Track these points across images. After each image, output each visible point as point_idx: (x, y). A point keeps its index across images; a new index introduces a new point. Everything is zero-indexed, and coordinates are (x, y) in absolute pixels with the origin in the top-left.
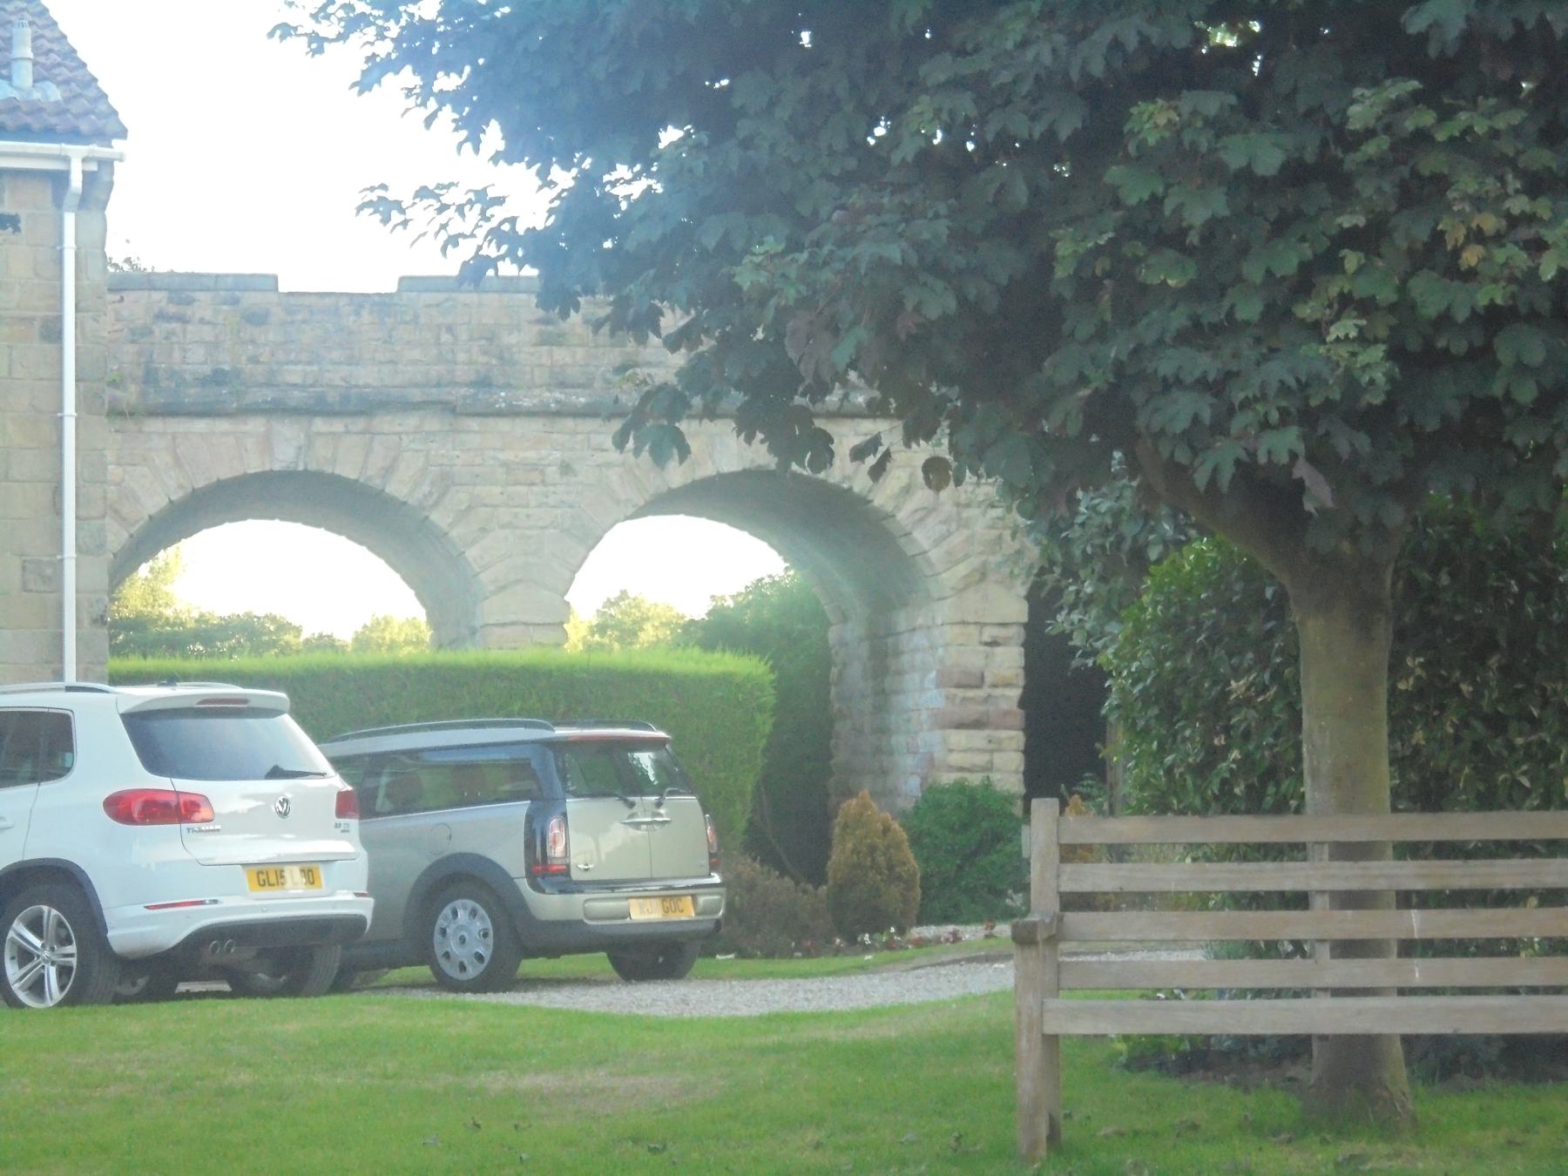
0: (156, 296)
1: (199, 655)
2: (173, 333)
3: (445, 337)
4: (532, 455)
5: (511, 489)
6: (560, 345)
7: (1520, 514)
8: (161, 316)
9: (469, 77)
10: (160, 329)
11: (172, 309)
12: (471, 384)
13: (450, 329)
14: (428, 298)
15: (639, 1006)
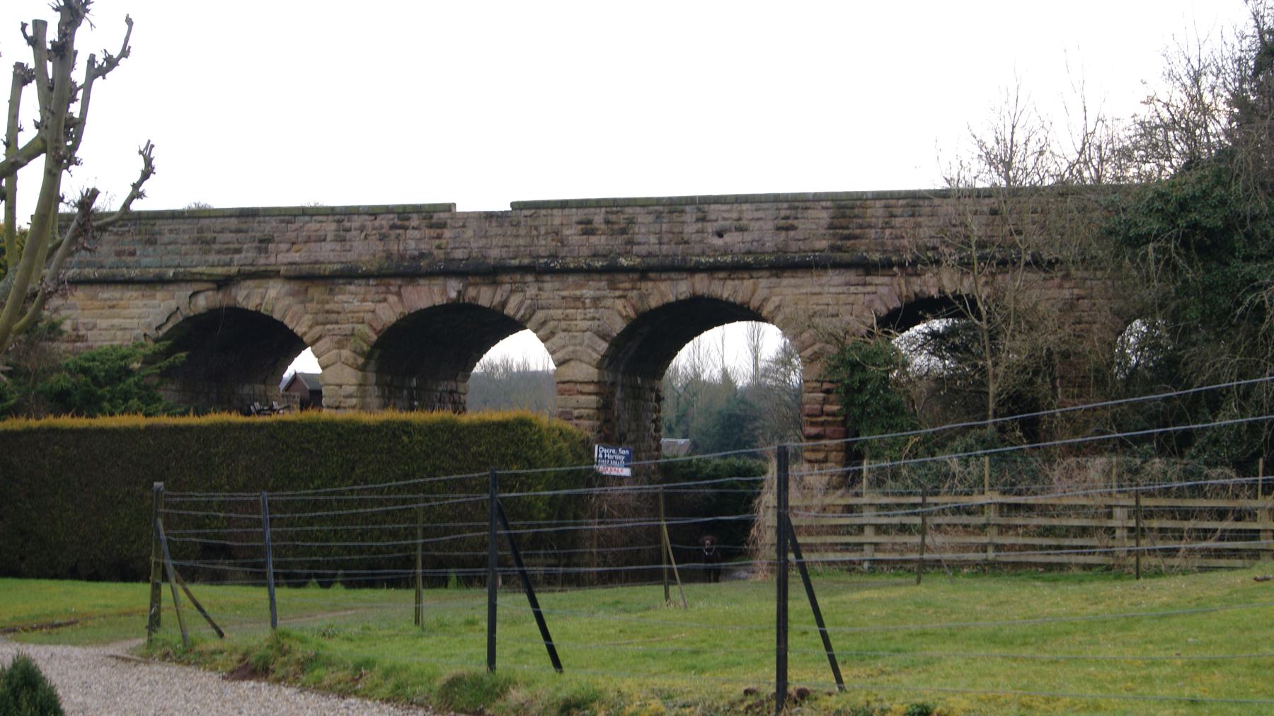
0: (391, 216)
1: (259, 412)
2: (399, 235)
3: (534, 233)
4: (578, 293)
5: (568, 311)
6: (594, 234)
7: (739, 664)
8: (393, 227)
9: (45, 42)
10: (393, 233)
11: (399, 223)
12: (548, 257)
13: (536, 228)
14: (527, 212)
15: (204, 686)
